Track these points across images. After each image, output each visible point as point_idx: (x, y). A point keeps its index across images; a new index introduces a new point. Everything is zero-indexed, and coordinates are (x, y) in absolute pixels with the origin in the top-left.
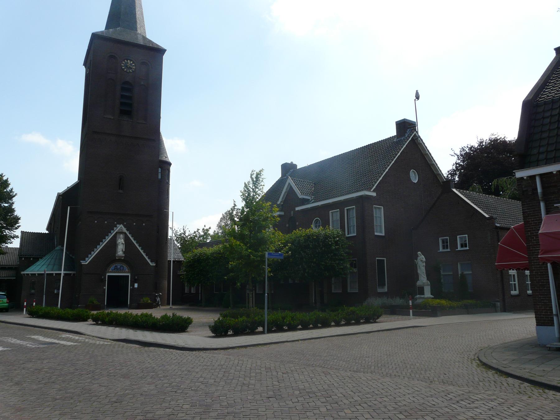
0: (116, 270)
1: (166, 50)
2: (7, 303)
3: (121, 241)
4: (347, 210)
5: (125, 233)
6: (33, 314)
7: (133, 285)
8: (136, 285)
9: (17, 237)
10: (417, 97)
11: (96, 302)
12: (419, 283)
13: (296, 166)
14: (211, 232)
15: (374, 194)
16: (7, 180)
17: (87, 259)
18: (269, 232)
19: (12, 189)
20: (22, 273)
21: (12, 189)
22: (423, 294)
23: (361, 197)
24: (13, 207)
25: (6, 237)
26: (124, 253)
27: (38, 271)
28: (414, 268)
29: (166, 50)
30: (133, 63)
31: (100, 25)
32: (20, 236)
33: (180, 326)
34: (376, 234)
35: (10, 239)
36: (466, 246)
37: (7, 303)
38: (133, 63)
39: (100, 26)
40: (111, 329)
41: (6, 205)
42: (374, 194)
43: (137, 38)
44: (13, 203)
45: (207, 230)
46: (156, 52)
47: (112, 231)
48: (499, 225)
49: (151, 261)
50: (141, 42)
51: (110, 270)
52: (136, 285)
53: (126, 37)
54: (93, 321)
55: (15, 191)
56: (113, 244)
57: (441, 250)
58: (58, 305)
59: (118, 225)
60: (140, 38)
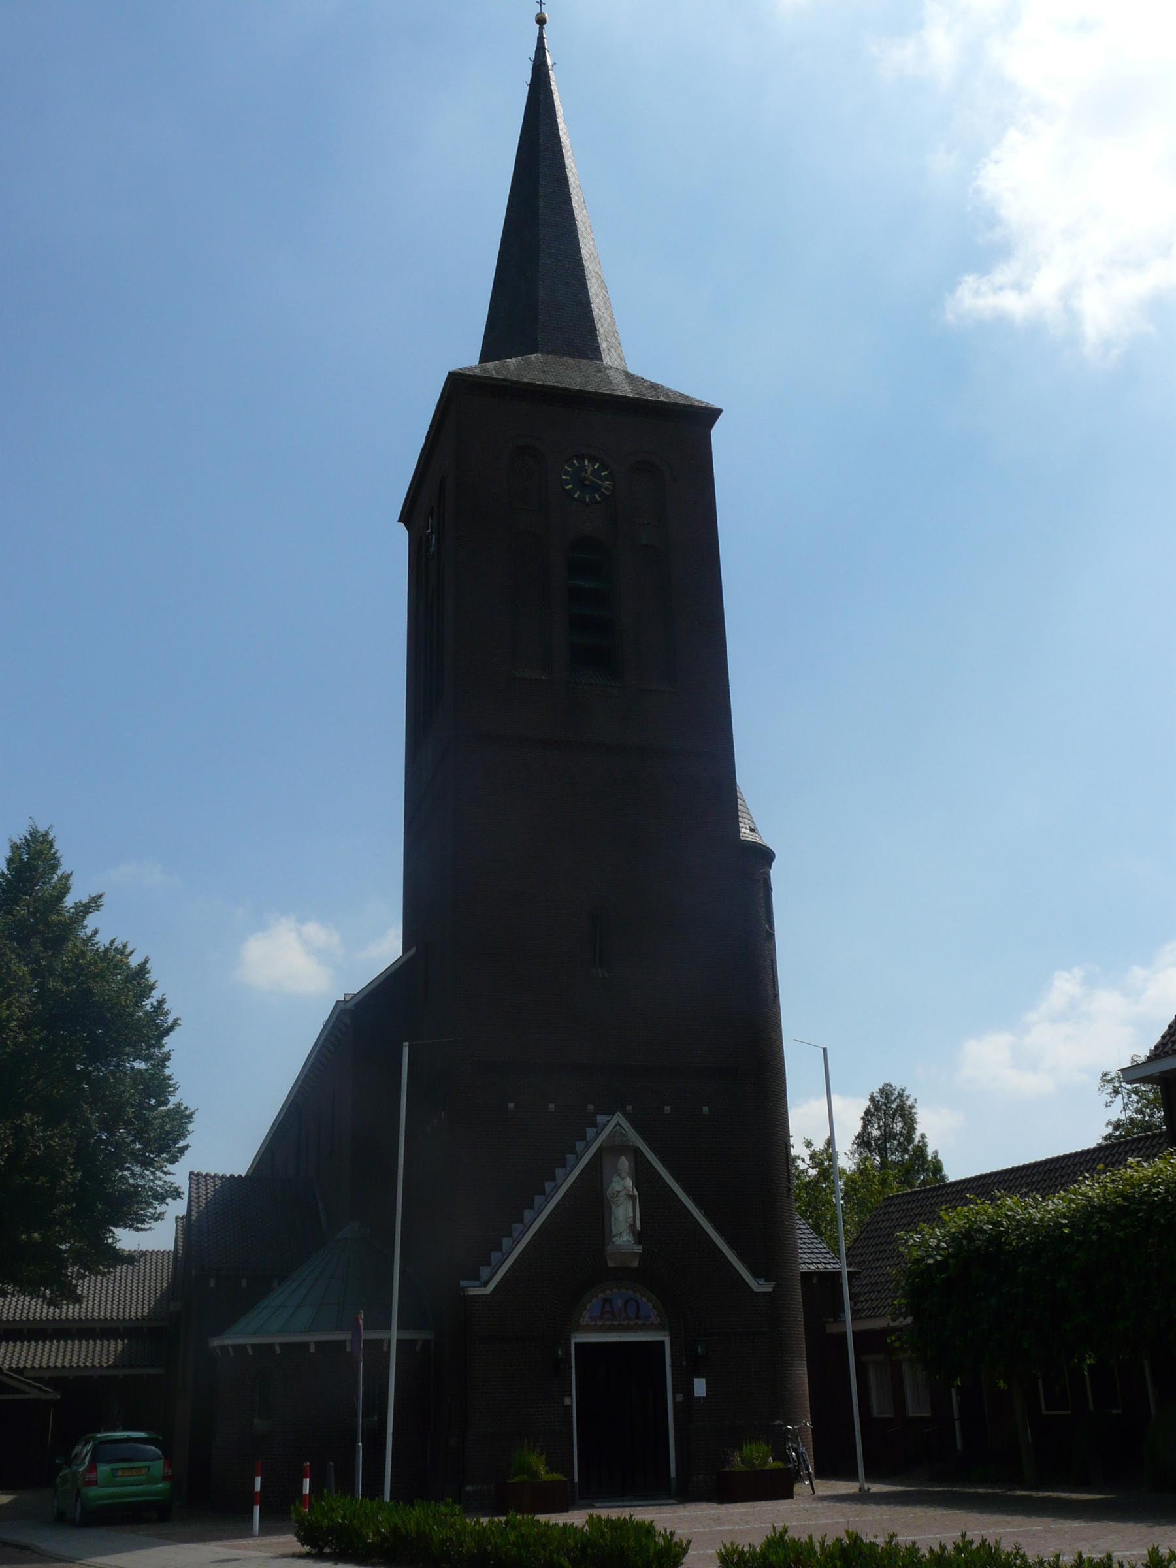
1: (717, 412)
2: (165, 1478)
3: (622, 1184)
5: (637, 1152)
8: (700, 1387)
9: (177, 1194)
11: (544, 1474)
14: (847, 1162)
16: (142, 969)
17: (485, 1272)
19: (161, 1002)
20: (216, 1342)
21: (161, 1002)
24: (167, 1072)
25: (137, 1194)
26: (639, 1237)
29: (717, 412)
30: (604, 467)
32: (185, 1189)
35: (149, 1204)
37: (165, 1478)
38: (604, 467)
39: (466, 354)
41: (140, 1065)
44: (166, 1057)
47: (580, 1146)
49: (756, 1275)
50: (627, 391)
51: (585, 1320)
52: (700, 1387)
53: (566, 374)
55: (174, 1009)
56: (590, 1201)
59: (601, 1119)
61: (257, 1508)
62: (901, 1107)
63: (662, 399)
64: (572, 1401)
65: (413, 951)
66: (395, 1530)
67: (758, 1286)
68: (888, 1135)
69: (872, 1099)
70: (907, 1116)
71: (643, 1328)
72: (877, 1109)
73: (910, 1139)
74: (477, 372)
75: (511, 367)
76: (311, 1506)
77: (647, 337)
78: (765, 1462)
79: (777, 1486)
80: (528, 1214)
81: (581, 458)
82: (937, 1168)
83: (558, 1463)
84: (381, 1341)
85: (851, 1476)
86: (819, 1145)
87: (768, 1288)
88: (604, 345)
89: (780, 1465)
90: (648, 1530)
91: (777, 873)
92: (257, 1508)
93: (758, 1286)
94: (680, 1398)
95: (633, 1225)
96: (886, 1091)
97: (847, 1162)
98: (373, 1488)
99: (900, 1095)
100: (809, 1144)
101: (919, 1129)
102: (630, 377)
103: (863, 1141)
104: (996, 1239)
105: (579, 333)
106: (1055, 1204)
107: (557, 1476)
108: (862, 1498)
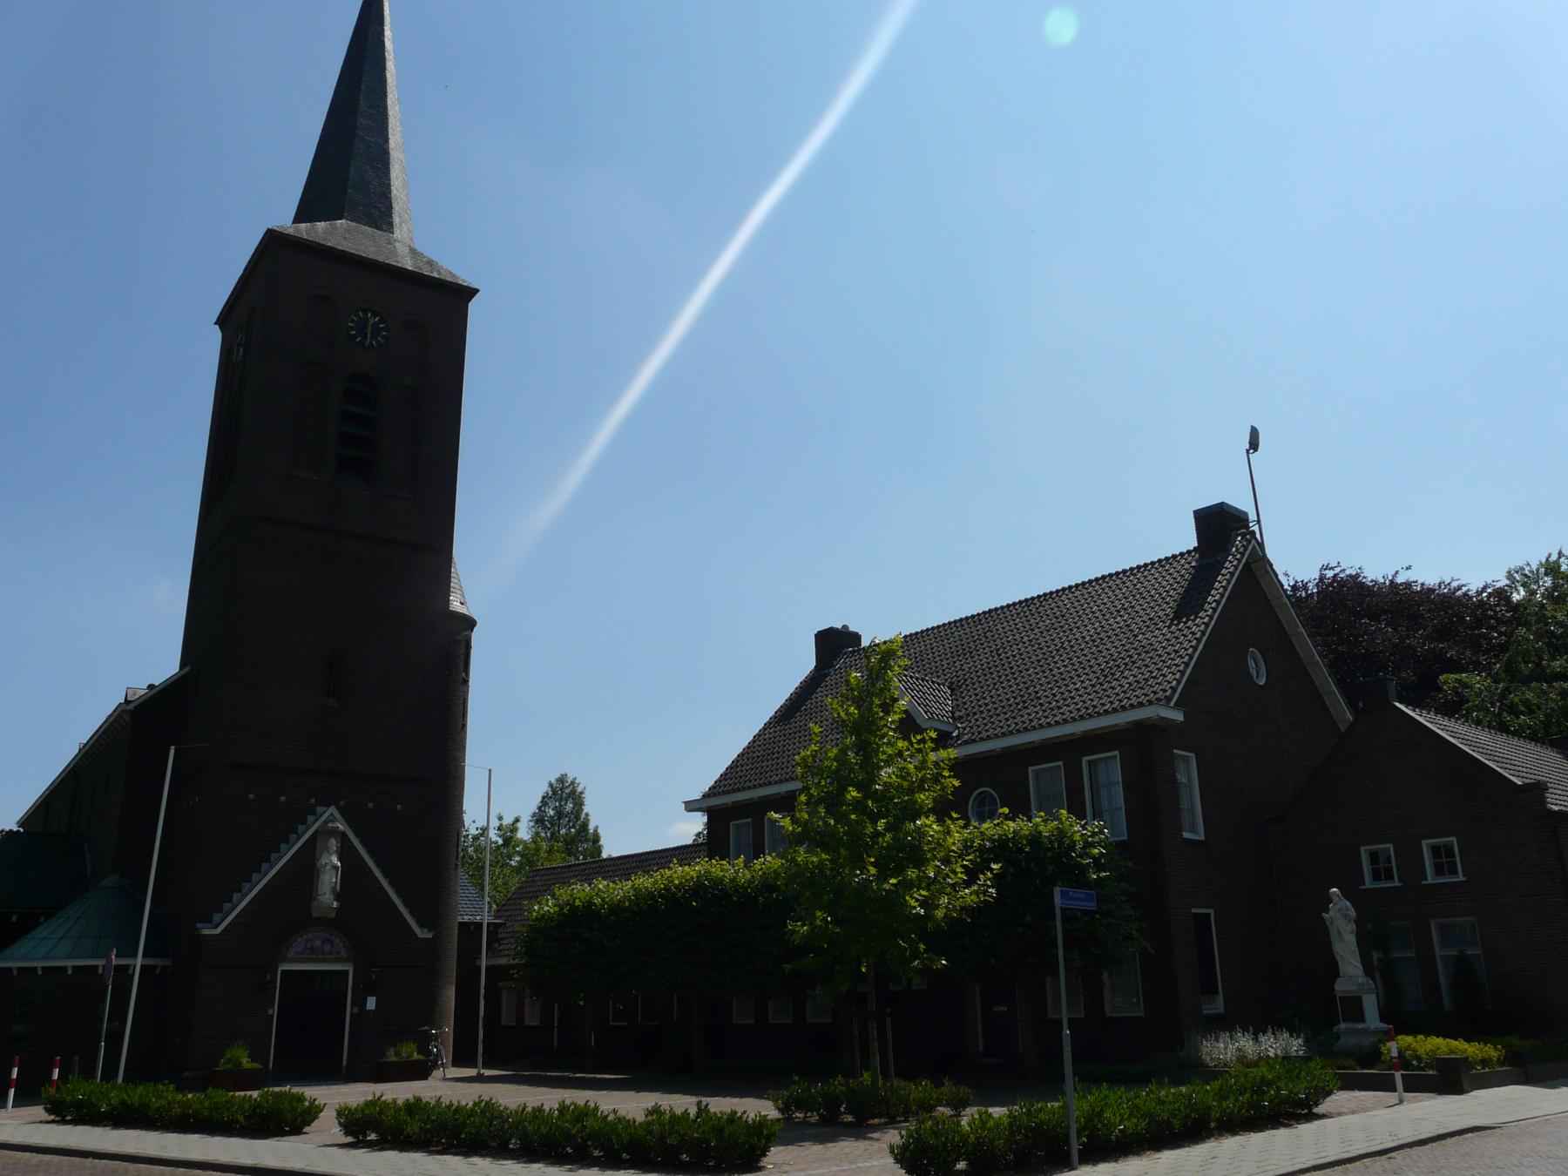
0: (312, 954)
1: (474, 292)
4: (1090, 762)
6: (64, 1112)
7: (360, 1002)
8: (371, 1003)
10: (1254, 445)
11: (246, 1063)
12: (1341, 987)
13: (856, 637)
14: (524, 833)
15: (1178, 716)
18: (1041, 828)
22: (1363, 1020)
23: (1140, 725)
26: (338, 897)
27: (46, 957)
28: (1322, 937)
29: (474, 292)
31: (279, 208)
33: (291, 1121)
34: (1186, 835)
36: (1390, 877)
38: (382, 320)
40: (98, 1131)
42: (1178, 716)
43: (394, 253)
45: (513, 828)
46: (452, 299)
48: (1555, 808)
49: (421, 926)
50: (409, 265)
52: (371, 1003)
54: (347, 1134)
56: (306, 866)
57: (1369, 883)
58: (116, 1076)
59: (319, 809)
60: (402, 249)
61: (12, 1092)
62: (573, 792)
63: (435, 275)
64: (274, 1012)
65: (187, 669)
66: (123, 1103)
67: (423, 934)
68: (560, 813)
69: (551, 785)
70: (577, 799)
71: (337, 960)
72: (554, 792)
73: (578, 817)
74: (291, 231)
75: (318, 231)
76: (58, 1088)
77: (430, 220)
78: (411, 1055)
79: (420, 1071)
80: (227, 906)
81: (365, 311)
82: (596, 839)
83: (258, 1054)
84: (128, 967)
85: (473, 1065)
86: (507, 821)
87: (430, 936)
88: (396, 220)
89: (421, 1057)
90: (301, 1098)
91: (477, 637)
92: (12, 1092)
93: (423, 934)
94: (356, 1010)
95: (334, 888)
96: (562, 780)
97: (524, 833)
98: (110, 1074)
99: (573, 783)
100: (500, 818)
101: (586, 809)
102: (413, 251)
103: (539, 819)
104: (589, 905)
105: (377, 209)
106: (644, 882)
107: (256, 1065)
108: (480, 1079)
